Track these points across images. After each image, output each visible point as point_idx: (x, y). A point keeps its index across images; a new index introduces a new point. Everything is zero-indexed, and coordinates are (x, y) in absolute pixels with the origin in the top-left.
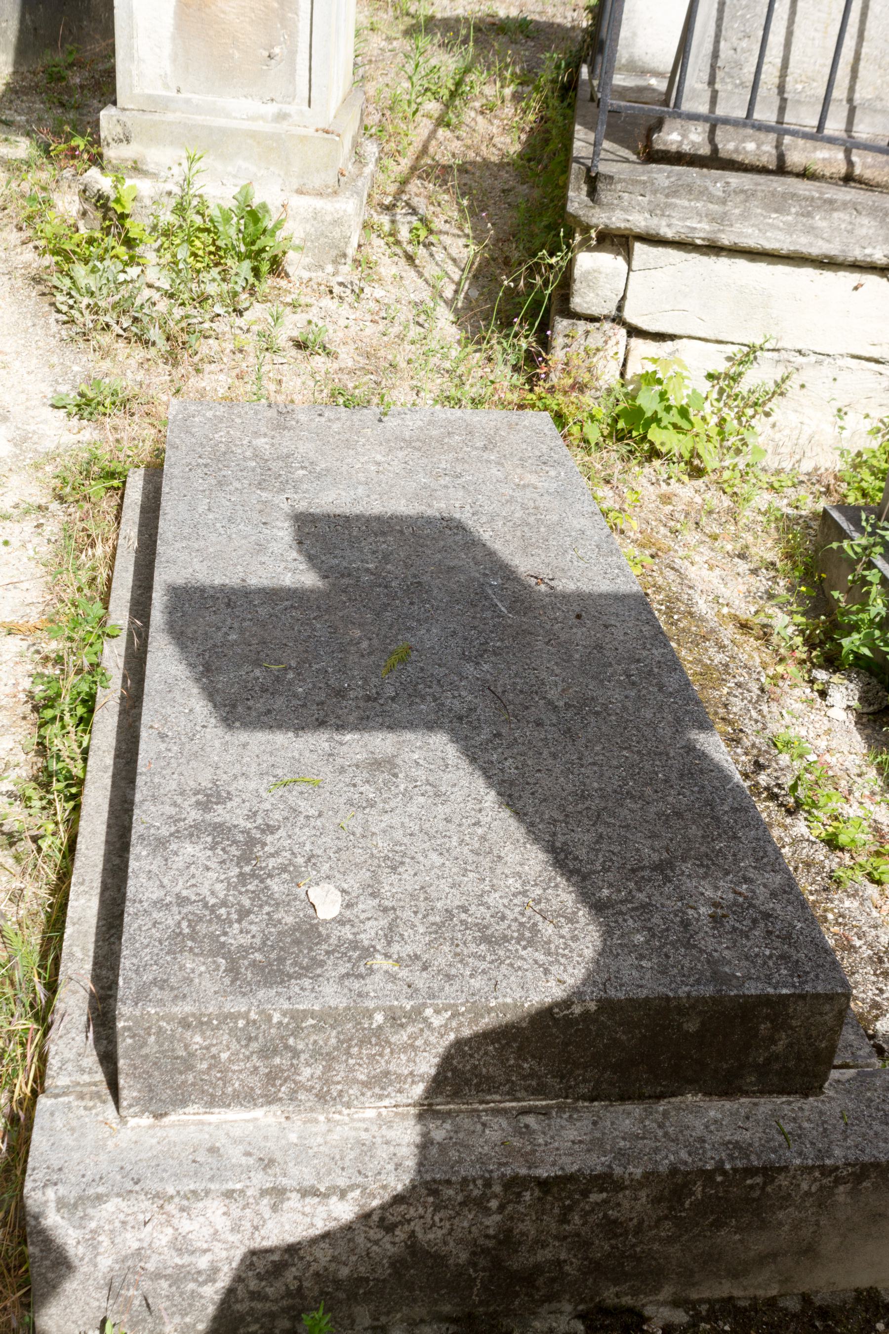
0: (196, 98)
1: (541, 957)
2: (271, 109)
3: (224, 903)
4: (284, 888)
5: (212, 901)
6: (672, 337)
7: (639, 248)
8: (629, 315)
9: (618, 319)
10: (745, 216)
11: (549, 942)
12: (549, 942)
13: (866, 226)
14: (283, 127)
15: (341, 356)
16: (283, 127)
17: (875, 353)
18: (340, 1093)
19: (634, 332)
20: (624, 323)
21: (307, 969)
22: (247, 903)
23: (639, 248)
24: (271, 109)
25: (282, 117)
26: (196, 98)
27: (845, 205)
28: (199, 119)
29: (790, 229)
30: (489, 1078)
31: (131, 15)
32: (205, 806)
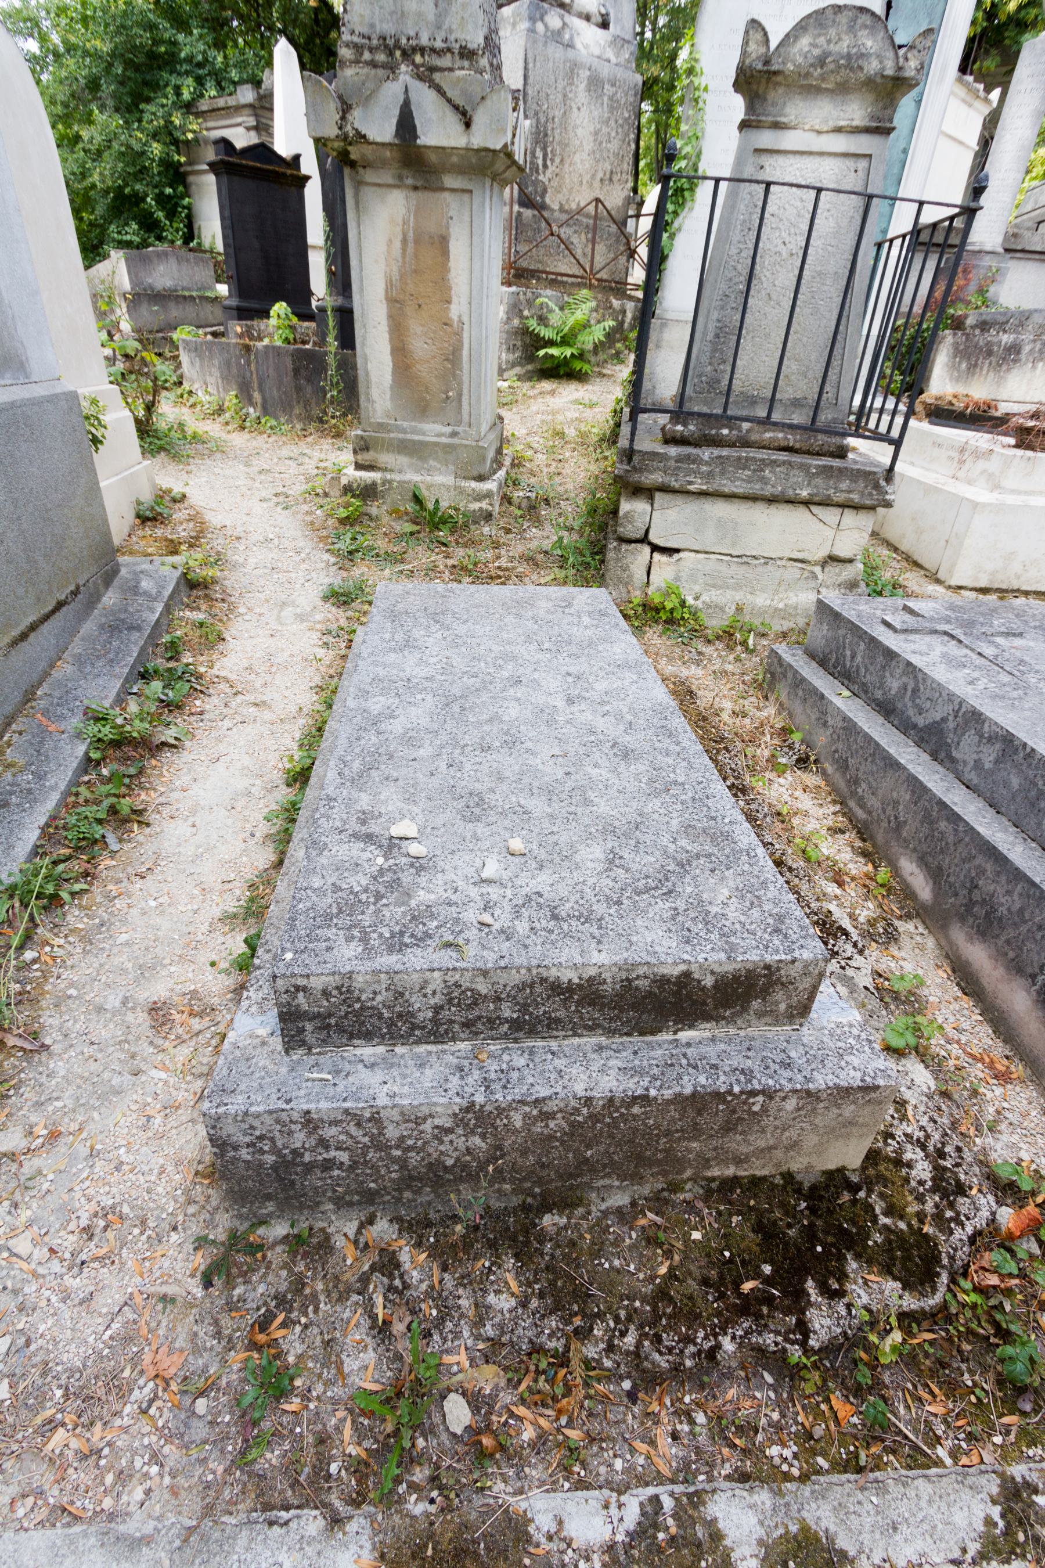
0: (405, 424)
1: (594, 930)
2: (448, 430)
3: (366, 890)
4: (410, 879)
5: (357, 889)
6: (677, 551)
7: (658, 495)
8: (653, 538)
9: (644, 540)
10: (723, 473)
11: (601, 919)
12: (601, 919)
13: (797, 477)
14: (455, 441)
15: (982, 1515)
16: (455, 441)
17: (800, 556)
18: (446, 1032)
19: (655, 548)
20: (650, 544)
21: (421, 939)
22: (382, 890)
23: (658, 495)
24: (448, 430)
25: (454, 434)
26: (405, 424)
27: (784, 463)
28: (409, 436)
29: (749, 481)
30: (558, 1021)
31: (367, 374)
32: (363, 822)
